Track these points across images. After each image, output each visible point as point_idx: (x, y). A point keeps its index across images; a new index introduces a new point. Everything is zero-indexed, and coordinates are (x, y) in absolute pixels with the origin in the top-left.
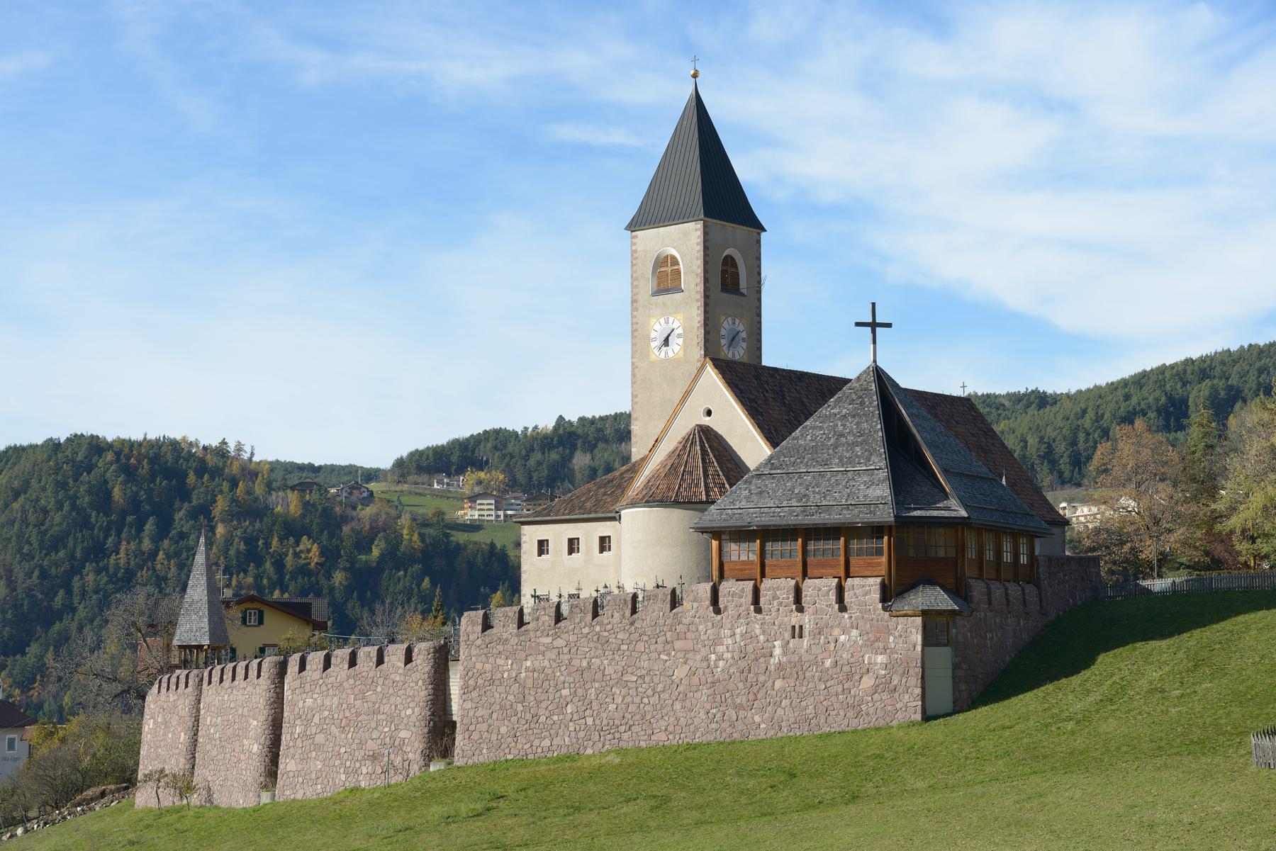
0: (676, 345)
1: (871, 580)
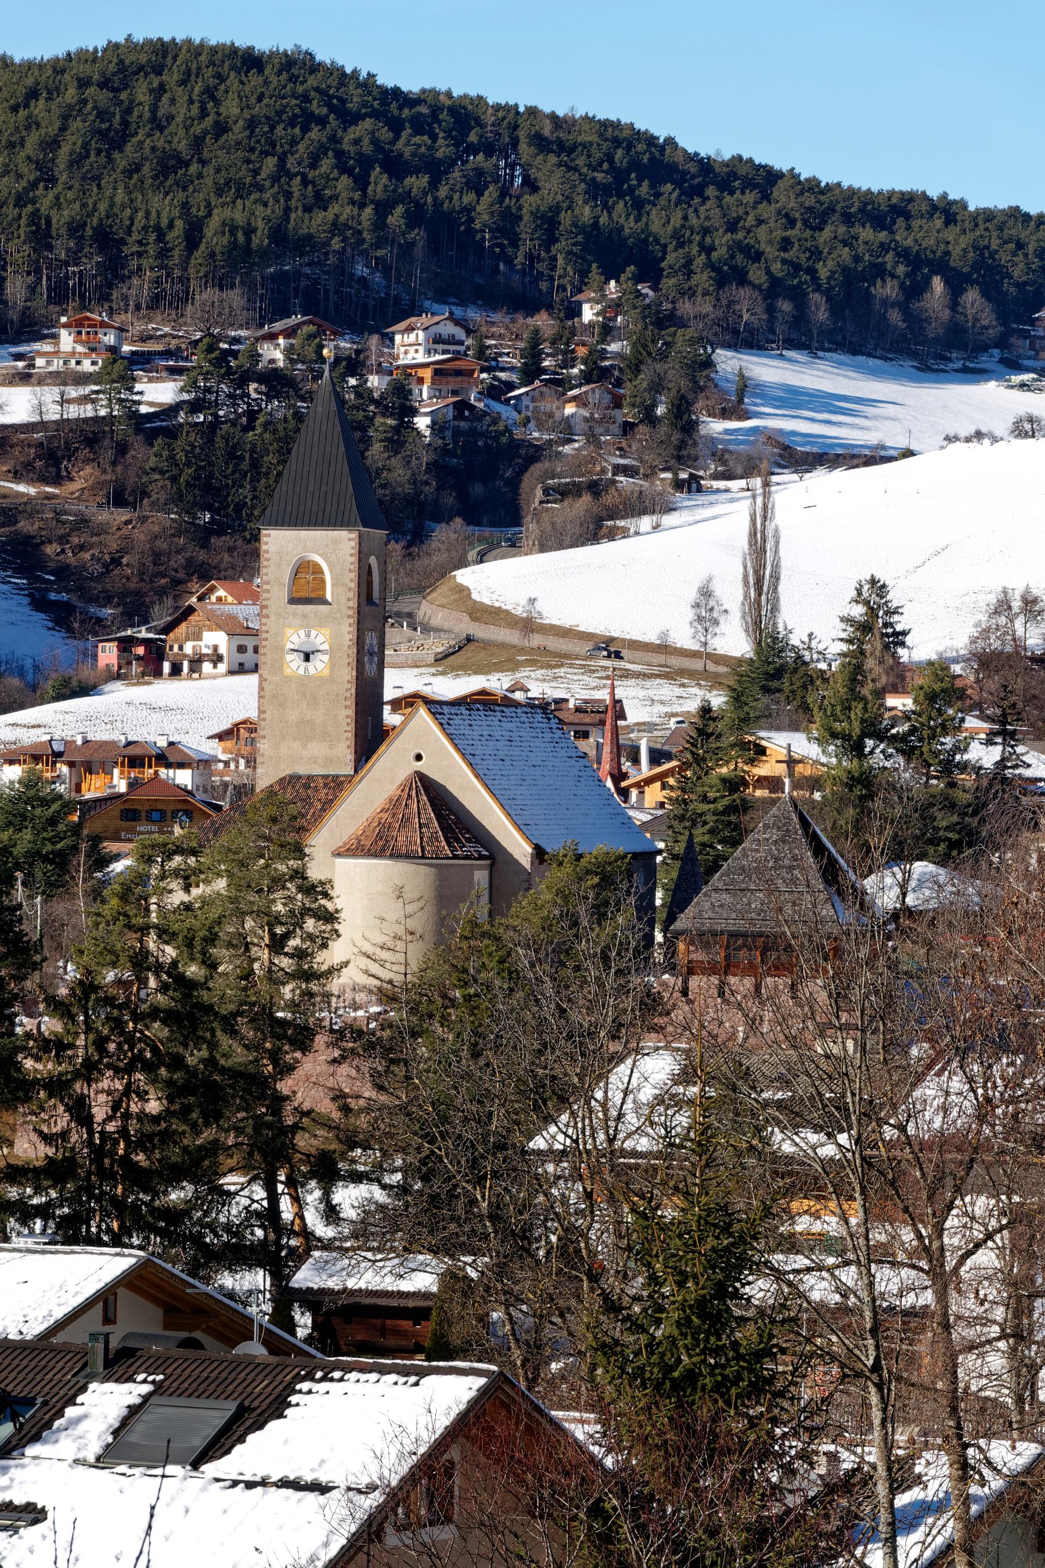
0: (319, 665)
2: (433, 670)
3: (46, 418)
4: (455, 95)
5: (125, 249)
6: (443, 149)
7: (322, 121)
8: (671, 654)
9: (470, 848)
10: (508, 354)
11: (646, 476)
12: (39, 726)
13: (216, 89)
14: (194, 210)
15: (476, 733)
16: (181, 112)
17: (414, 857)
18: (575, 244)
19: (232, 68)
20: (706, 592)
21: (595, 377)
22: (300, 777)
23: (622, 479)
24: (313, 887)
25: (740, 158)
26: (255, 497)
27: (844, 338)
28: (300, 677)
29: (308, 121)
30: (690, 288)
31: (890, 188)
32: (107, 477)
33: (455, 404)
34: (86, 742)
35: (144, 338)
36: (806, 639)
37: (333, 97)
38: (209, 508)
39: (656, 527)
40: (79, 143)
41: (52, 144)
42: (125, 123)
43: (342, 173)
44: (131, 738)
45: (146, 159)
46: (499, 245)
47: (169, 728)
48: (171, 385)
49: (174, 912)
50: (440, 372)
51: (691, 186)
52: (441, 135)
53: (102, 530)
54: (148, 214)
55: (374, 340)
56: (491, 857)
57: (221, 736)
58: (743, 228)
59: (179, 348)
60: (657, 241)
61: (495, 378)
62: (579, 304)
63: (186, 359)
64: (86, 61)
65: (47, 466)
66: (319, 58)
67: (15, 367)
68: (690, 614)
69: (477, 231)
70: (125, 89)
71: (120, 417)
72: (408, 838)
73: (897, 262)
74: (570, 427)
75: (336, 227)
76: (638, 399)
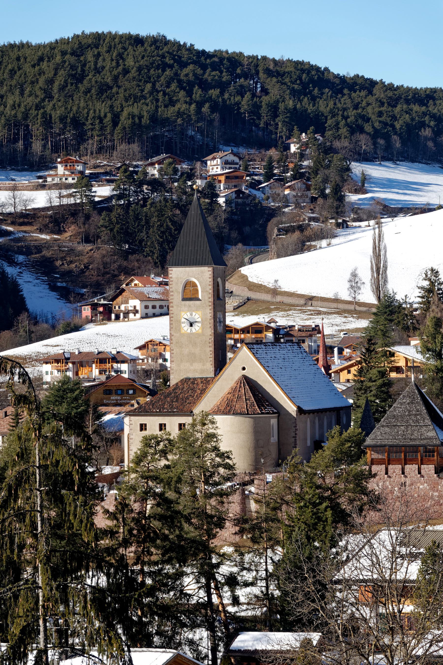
0: (197, 328)
1: (431, 466)
2: (233, 314)
3: (53, 205)
4: (229, 52)
5: (85, 127)
6: (226, 77)
7: (171, 67)
8: (339, 303)
9: (269, 409)
10: (258, 168)
11: (323, 222)
12: (58, 346)
13: (123, 54)
14: (115, 109)
15: (269, 356)
16: (108, 65)
17: (244, 414)
18: (286, 118)
19: (130, 44)
20: (354, 275)
21: (298, 177)
22: (190, 379)
23: (313, 223)
24: (223, 454)
25: (358, 76)
26: (148, 237)
27: (408, 155)
28: (188, 334)
29: (164, 66)
30: (339, 135)
31: (425, 87)
32: (82, 230)
33: (236, 192)
34: (80, 353)
35: (96, 167)
36: (404, 298)
37: (176, 55)
38: (127, 242)
39: (329, 245)
40: (63, 81)
41: (51, 82)
42: (83, 71)
43: (180, 90)
44: (100, 350)
45: (93, 86)
46: (252, 119)
47: (116, 345)
48: (108, 187)
49: (162, 469)
50: (228, 177)
51: (337, 89)
52: (225, 70)
53: (80, 254)
54: (95, 111)
55: (198, 165)
56: (278, 413)
57: (141, 348)
58: (361, 107)
59: (111, 171)
60: (323, 115)
61: (253, 179)
62: (289, 145)
63: (115, 175)
64: (65, 43)
65: (54, 226)
66: (168, 38)
67: (38, 182)
68: (348, 285)
69: (242, 113)
70: (82, 55)
71: (86, 203)
72: (241, 406)
73: (430, 120)
74: (287, 200)
75: (179, 114)
76: (318, 186)
